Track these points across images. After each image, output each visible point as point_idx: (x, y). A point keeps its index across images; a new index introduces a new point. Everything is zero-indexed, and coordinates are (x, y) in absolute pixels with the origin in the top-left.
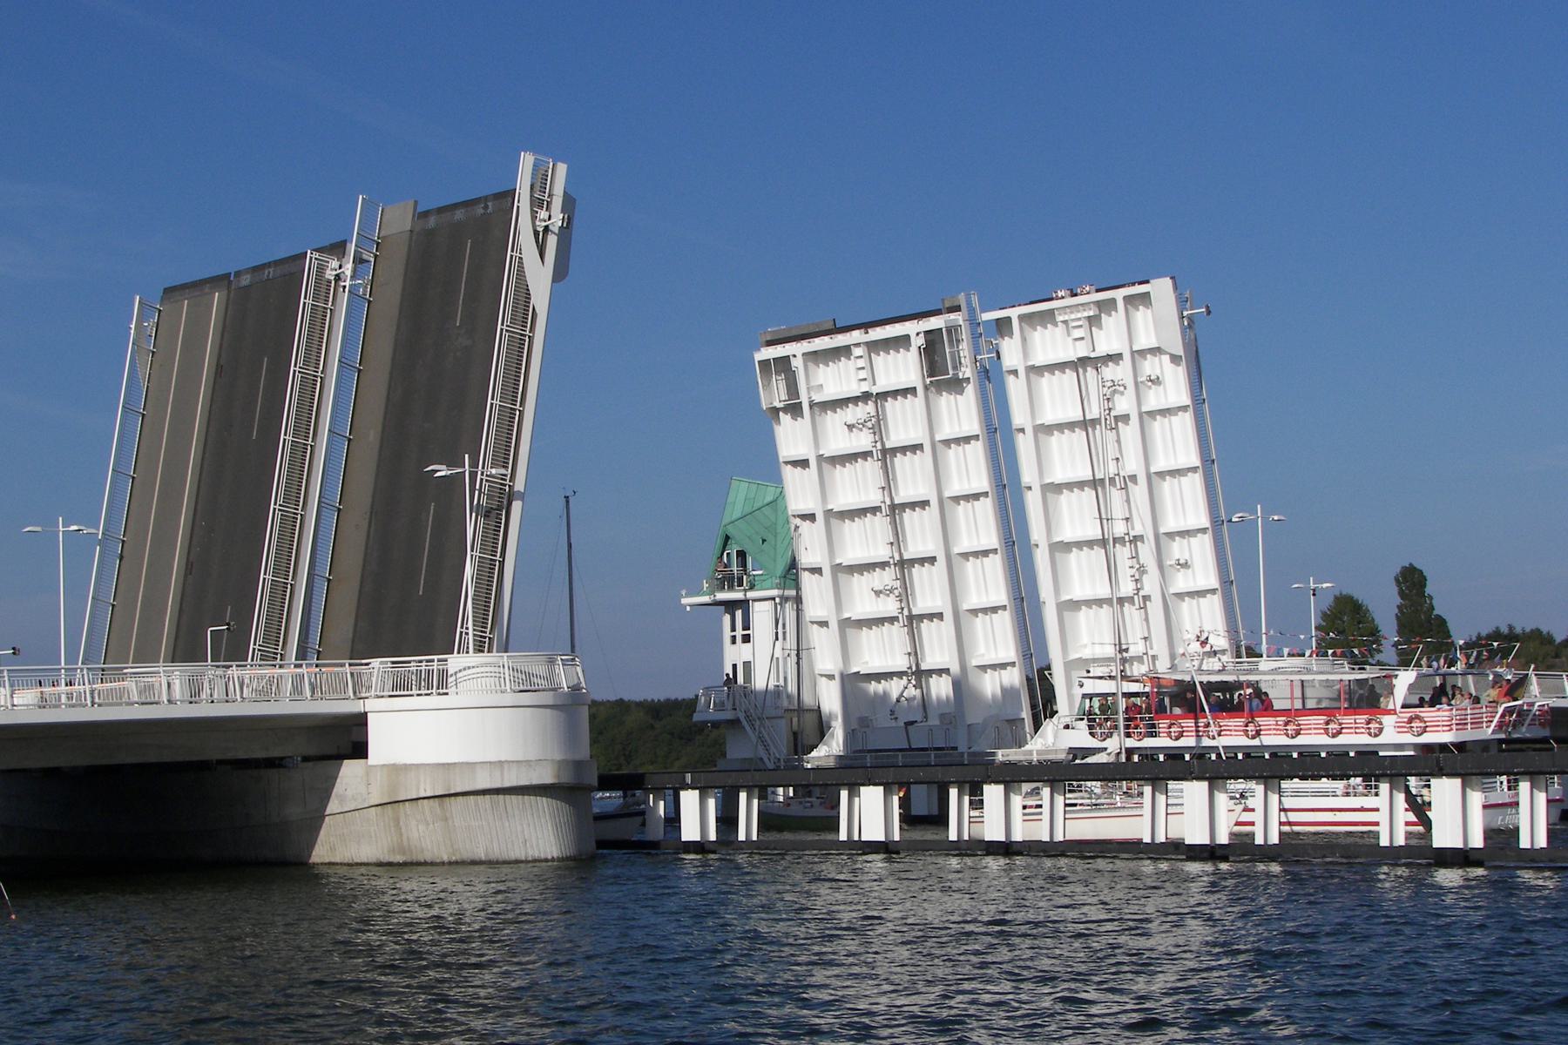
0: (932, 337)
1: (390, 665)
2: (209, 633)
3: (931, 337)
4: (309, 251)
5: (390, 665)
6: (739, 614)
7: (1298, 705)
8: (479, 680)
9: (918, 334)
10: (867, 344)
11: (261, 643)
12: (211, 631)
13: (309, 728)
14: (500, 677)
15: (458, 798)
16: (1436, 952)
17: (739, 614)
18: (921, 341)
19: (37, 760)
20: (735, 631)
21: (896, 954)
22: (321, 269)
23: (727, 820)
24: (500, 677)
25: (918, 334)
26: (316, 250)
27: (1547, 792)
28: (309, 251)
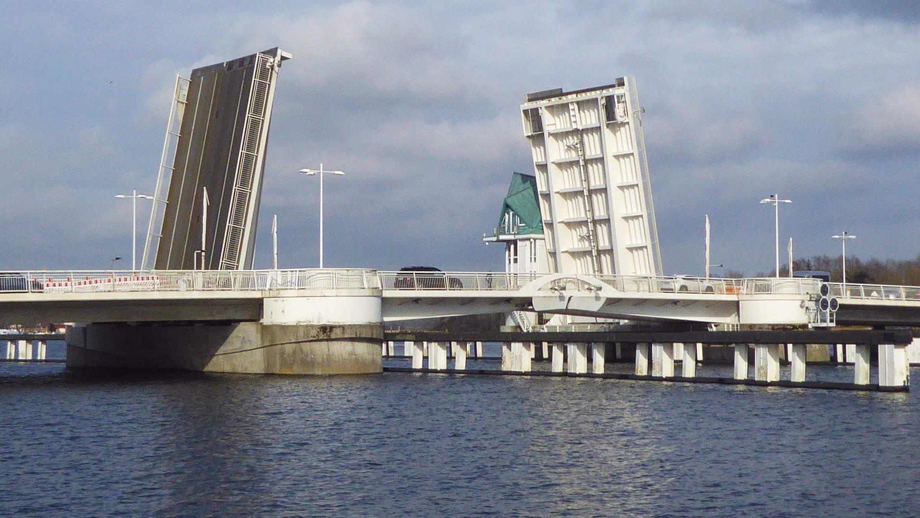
0: (610, 100)
1: (396, 274)
2: (195, 254)
3: (608, 99)
4: (258, 53)
5: (396, 274)
6: (512, 247)
7: (263, 291)
8: (325, 280)
9: (602, 98)
10: (578, 103)
11: (226, 260)
12: (197, 253)
13: (382, 307)
14: (330, 279)
15: (311, 343)
16: (125, 483)
17: (512, 247)
18: (604, 101)
19: (135, 319)
20: (517, 255)
21: (812, 430)
22: (264, 63)
23: (451, 358)
24: (330, 279)
25: (602, 98)
26: (262, 53)
27: (46, 361)
28: (258, 53)
